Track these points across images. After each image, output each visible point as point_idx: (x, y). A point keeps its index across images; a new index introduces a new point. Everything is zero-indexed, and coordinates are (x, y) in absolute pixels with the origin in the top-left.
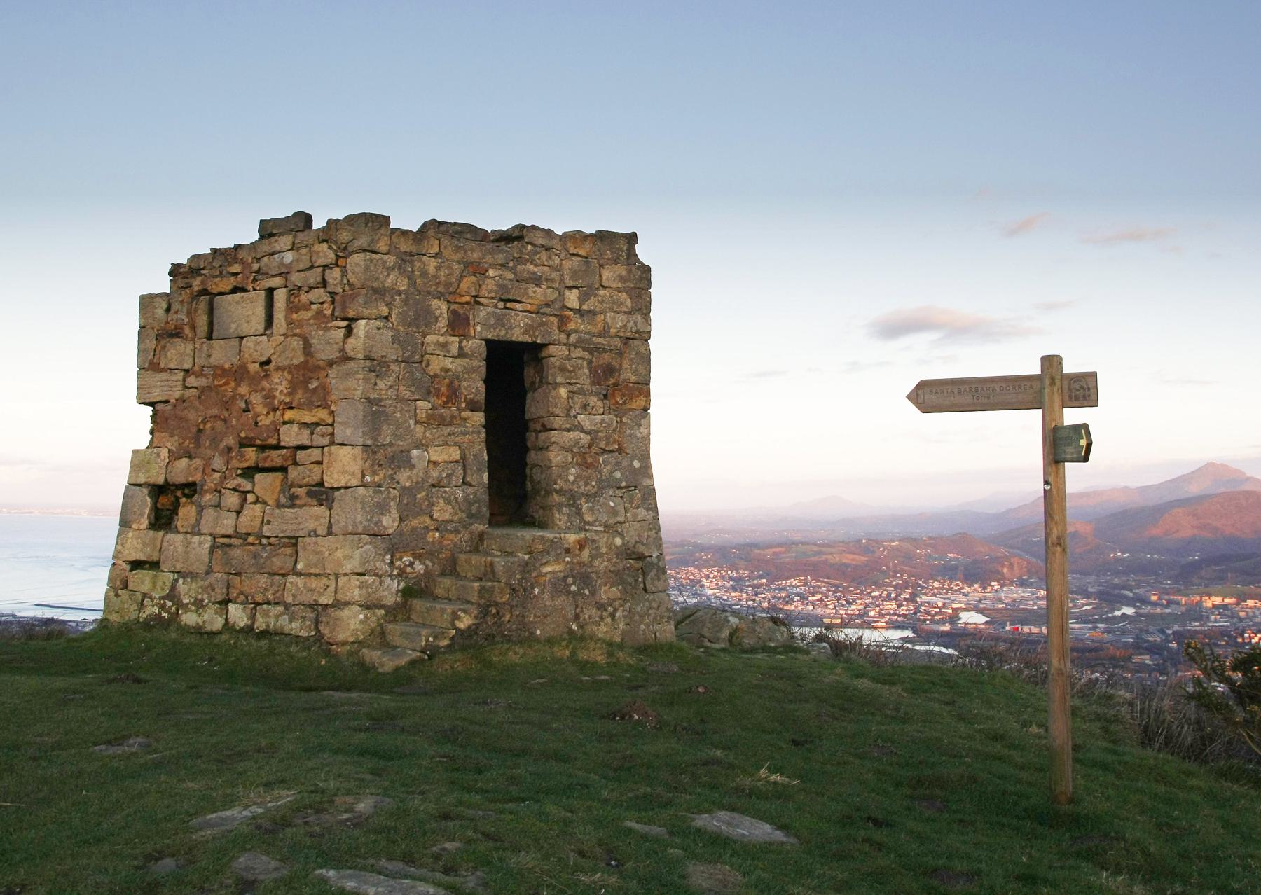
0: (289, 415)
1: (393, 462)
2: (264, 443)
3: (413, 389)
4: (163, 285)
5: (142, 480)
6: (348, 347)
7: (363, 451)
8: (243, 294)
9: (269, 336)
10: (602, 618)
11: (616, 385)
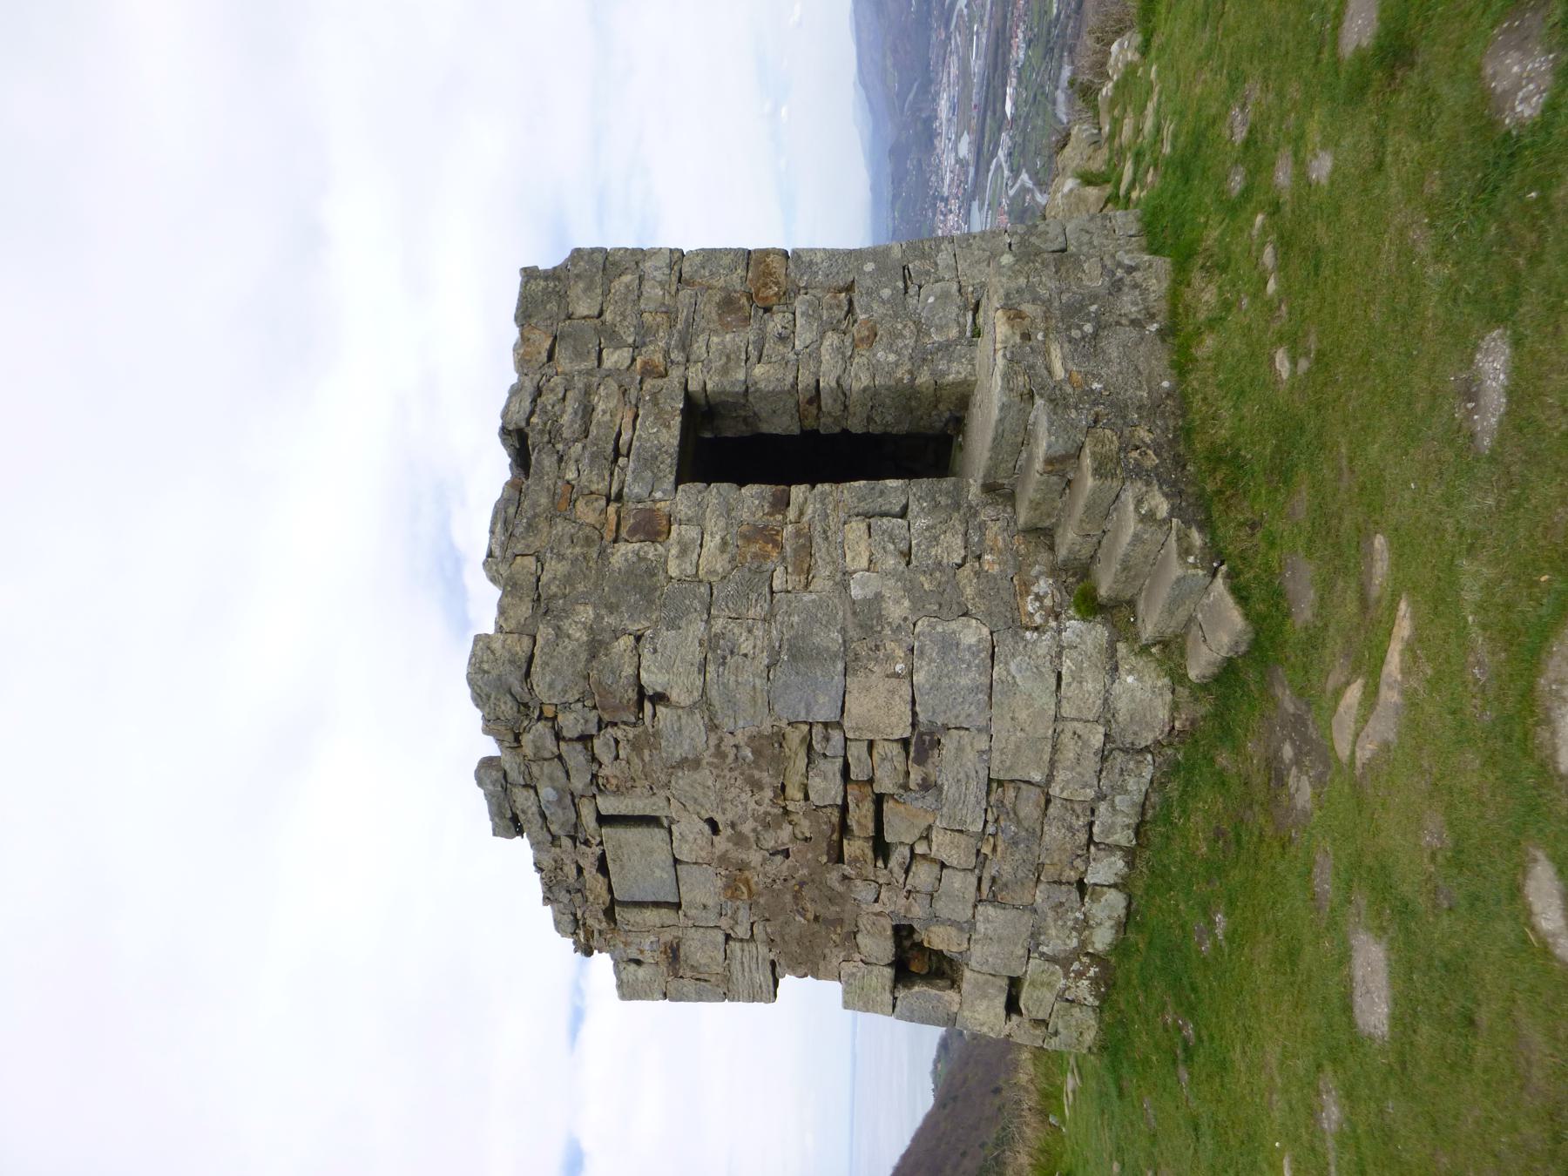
0: (794, 792)
1: (872, 628)
2: (837, 828)
3: (753, 596)
4: (602, 962)
5: (888, 997)
6: (685, 700)
7: (855, 674)
8: (608, 859)
9: (672, 821)
10: (1136, 286)
11: (750, 297)
